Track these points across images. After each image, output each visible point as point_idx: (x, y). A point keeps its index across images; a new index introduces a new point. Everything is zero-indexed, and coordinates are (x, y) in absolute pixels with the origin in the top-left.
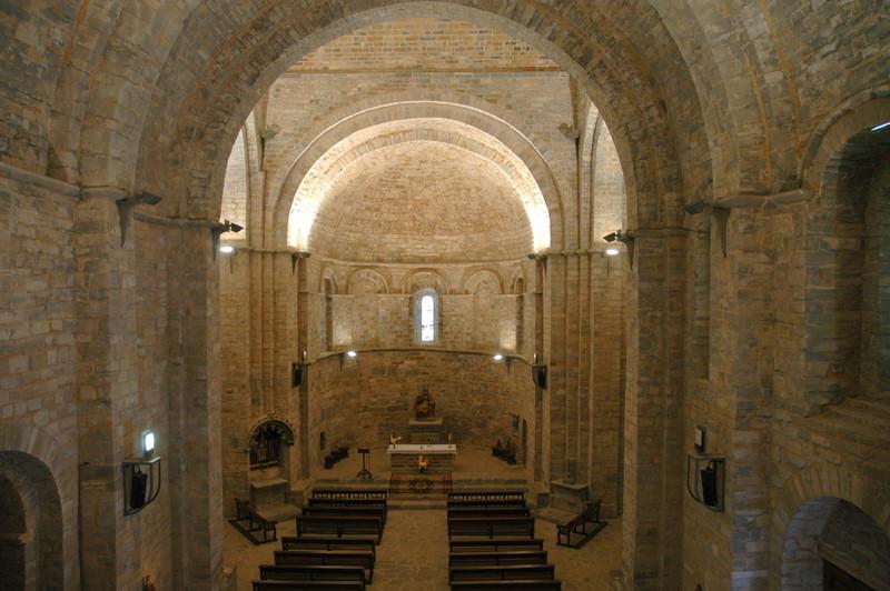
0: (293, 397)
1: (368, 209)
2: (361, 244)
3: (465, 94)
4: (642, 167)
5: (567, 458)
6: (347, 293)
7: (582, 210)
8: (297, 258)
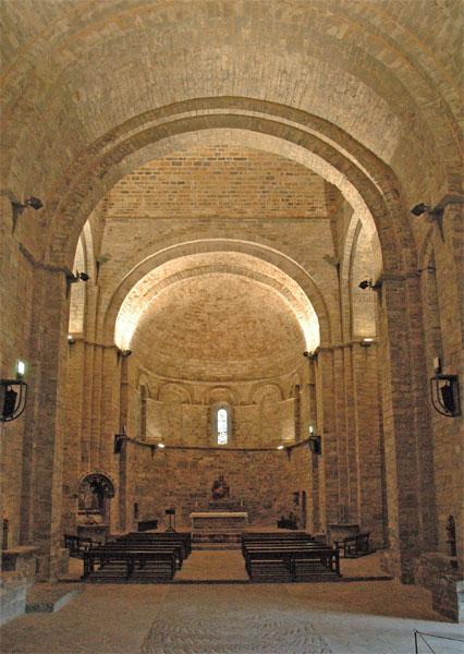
0: (114, 460)
1: (175, 336)
6: (158, 399)
7: (344, 315)
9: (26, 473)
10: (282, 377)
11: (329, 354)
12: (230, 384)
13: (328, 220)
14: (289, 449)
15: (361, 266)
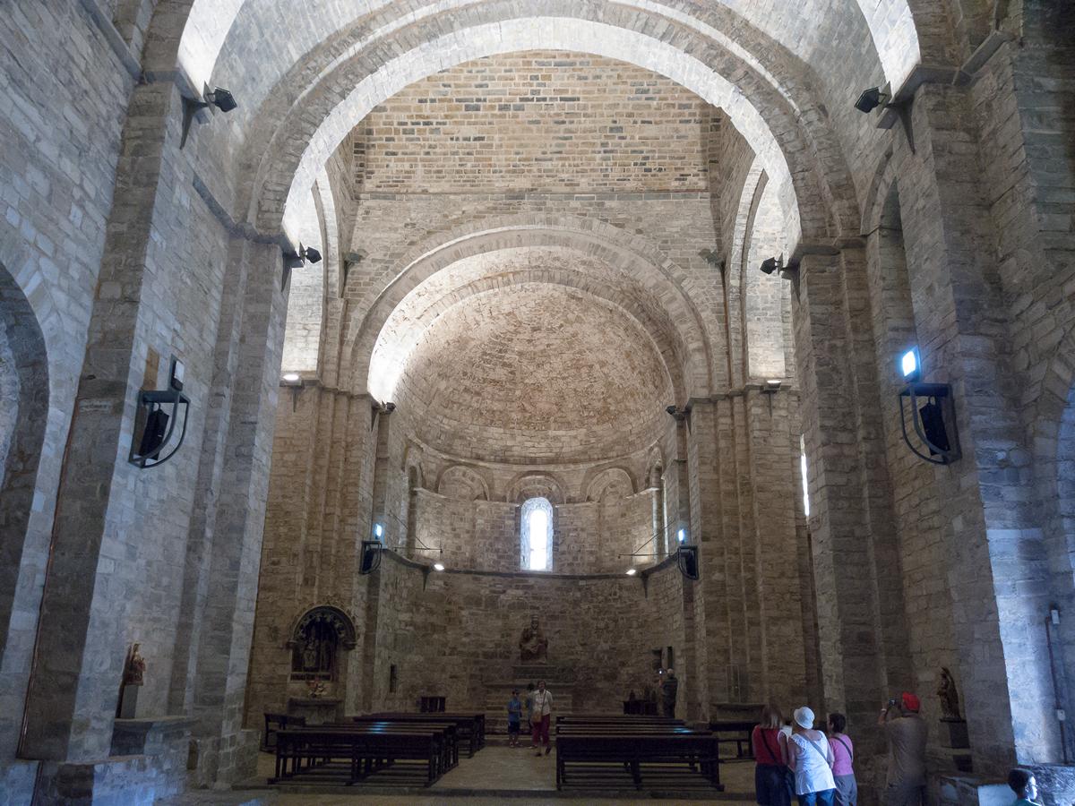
0: (358, 585)
1: (466, 390)
2: (454, 435)
3: (587, 218)
4: (803, 179)
8: (381, 413)
9: (189, 584)
11: (709, 409)
12: (551, 468)
13: (708, 194)
14: (644, 574)
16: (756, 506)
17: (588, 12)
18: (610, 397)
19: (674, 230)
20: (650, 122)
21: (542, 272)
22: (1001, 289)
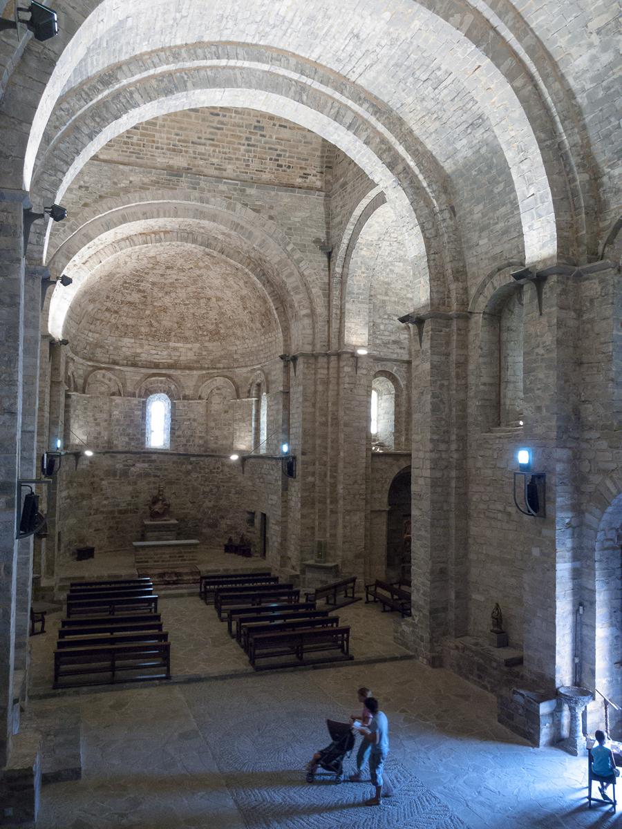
1: (108, 310)
2: (97, 345)
3: (232, 201)
4: (434, 260)
5: (317, 539)
6: (84, 393)
8: (54, 345)
10: (238, 371)
12: (171, 372)
13: (323, 194)
15: (359, 260)
16: (342, 436)
17: (295, 92)
18: (221, 323)
19: (297, 219)
20: (285, 127)
21: (188, 236)
22: (579, 419)
